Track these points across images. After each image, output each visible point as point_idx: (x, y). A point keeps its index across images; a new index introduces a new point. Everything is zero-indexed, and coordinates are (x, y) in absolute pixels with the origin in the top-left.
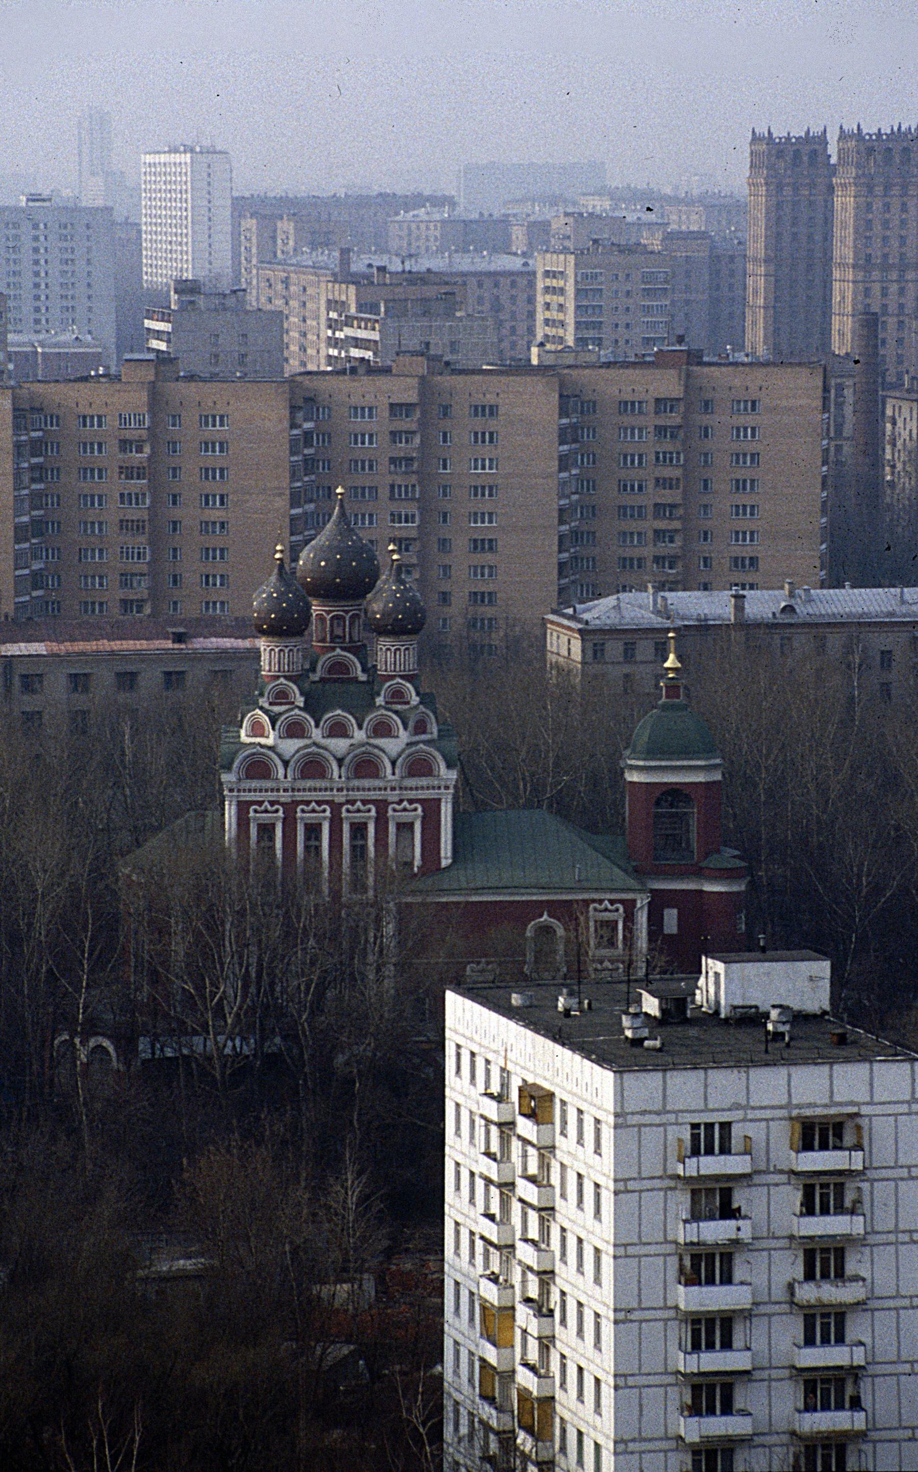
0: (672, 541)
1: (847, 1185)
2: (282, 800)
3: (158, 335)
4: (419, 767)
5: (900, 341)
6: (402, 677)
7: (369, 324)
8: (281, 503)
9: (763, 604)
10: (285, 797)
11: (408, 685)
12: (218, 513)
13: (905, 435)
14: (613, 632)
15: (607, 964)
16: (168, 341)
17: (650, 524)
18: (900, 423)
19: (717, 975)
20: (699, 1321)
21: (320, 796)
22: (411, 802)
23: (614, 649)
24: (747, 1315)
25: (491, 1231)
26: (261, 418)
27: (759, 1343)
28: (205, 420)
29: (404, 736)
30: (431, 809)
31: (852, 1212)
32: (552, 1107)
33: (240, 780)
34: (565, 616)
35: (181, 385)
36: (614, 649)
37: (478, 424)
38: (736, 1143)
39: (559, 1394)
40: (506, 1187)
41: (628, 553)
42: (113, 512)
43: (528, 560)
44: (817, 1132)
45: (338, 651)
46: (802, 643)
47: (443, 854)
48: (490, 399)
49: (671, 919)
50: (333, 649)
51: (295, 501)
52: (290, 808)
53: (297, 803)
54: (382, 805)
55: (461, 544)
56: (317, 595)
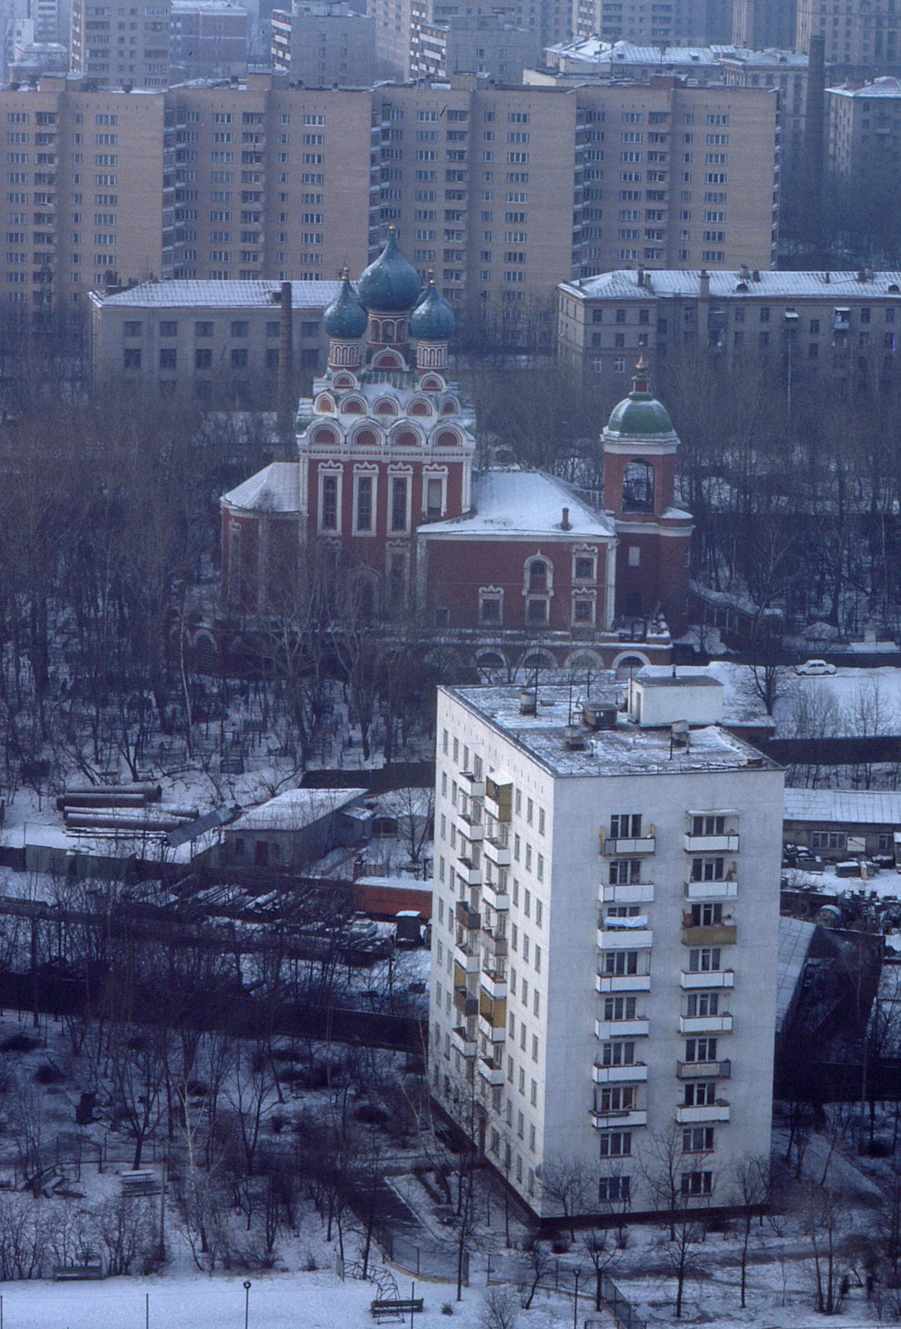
0: (659, 218)
1: (725, 860)
2: (343, 459)
3: (280, 32)
4: (447, 438)
5: (848, 45)
6: (435, 371)
7: (440, 34)
8: (364, 182)
9: (724, 283)
10: (345, 458)
11: (441, 377)
12: (316, 188)
13: (844, 137)
14: (607, 301)
15: (584, 590)
16: (289, 38)
17: (643, 205)
18: (840, 128)
19: (639, 694)
20: (612, 955)
21: (372, 458)
22: (440, 464)
23: (609, 315)
24: (649, 951)
25: (464, 872)
26: (346, 128)
27: (658, 971)
28: (307, 119)
29: (435, 416)
30: (455, 470)
31: (730, 879)
32: (510, 794)
33: (311, 443)
34: (572, 285)
35: (292, 91)
36: (609, 315)
37: (514, 127)
38: (644, 832)
39: (510, 996)
40: (476, 843)
41: (627, 225)
42: (237, 187)
43: (551, 231)
44: (703, 825)
45: (388, 348)
46: (753, 315)
47: (463, 504)
48: (524, 110)
49: (634, 555)
50: (385, 347)
51: (373, 180)
52: (348, 467)
53: (353, 462)
54: (418, 467)
55: (499, 215)
56: (373, 306)
